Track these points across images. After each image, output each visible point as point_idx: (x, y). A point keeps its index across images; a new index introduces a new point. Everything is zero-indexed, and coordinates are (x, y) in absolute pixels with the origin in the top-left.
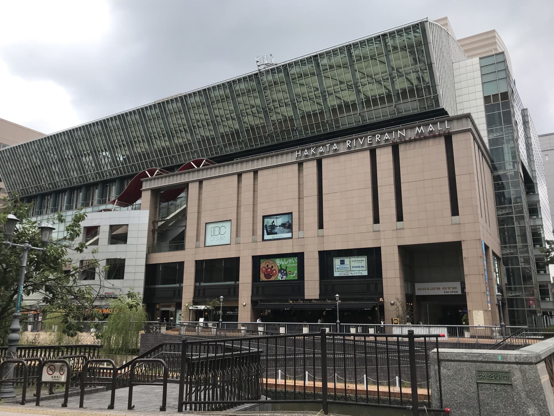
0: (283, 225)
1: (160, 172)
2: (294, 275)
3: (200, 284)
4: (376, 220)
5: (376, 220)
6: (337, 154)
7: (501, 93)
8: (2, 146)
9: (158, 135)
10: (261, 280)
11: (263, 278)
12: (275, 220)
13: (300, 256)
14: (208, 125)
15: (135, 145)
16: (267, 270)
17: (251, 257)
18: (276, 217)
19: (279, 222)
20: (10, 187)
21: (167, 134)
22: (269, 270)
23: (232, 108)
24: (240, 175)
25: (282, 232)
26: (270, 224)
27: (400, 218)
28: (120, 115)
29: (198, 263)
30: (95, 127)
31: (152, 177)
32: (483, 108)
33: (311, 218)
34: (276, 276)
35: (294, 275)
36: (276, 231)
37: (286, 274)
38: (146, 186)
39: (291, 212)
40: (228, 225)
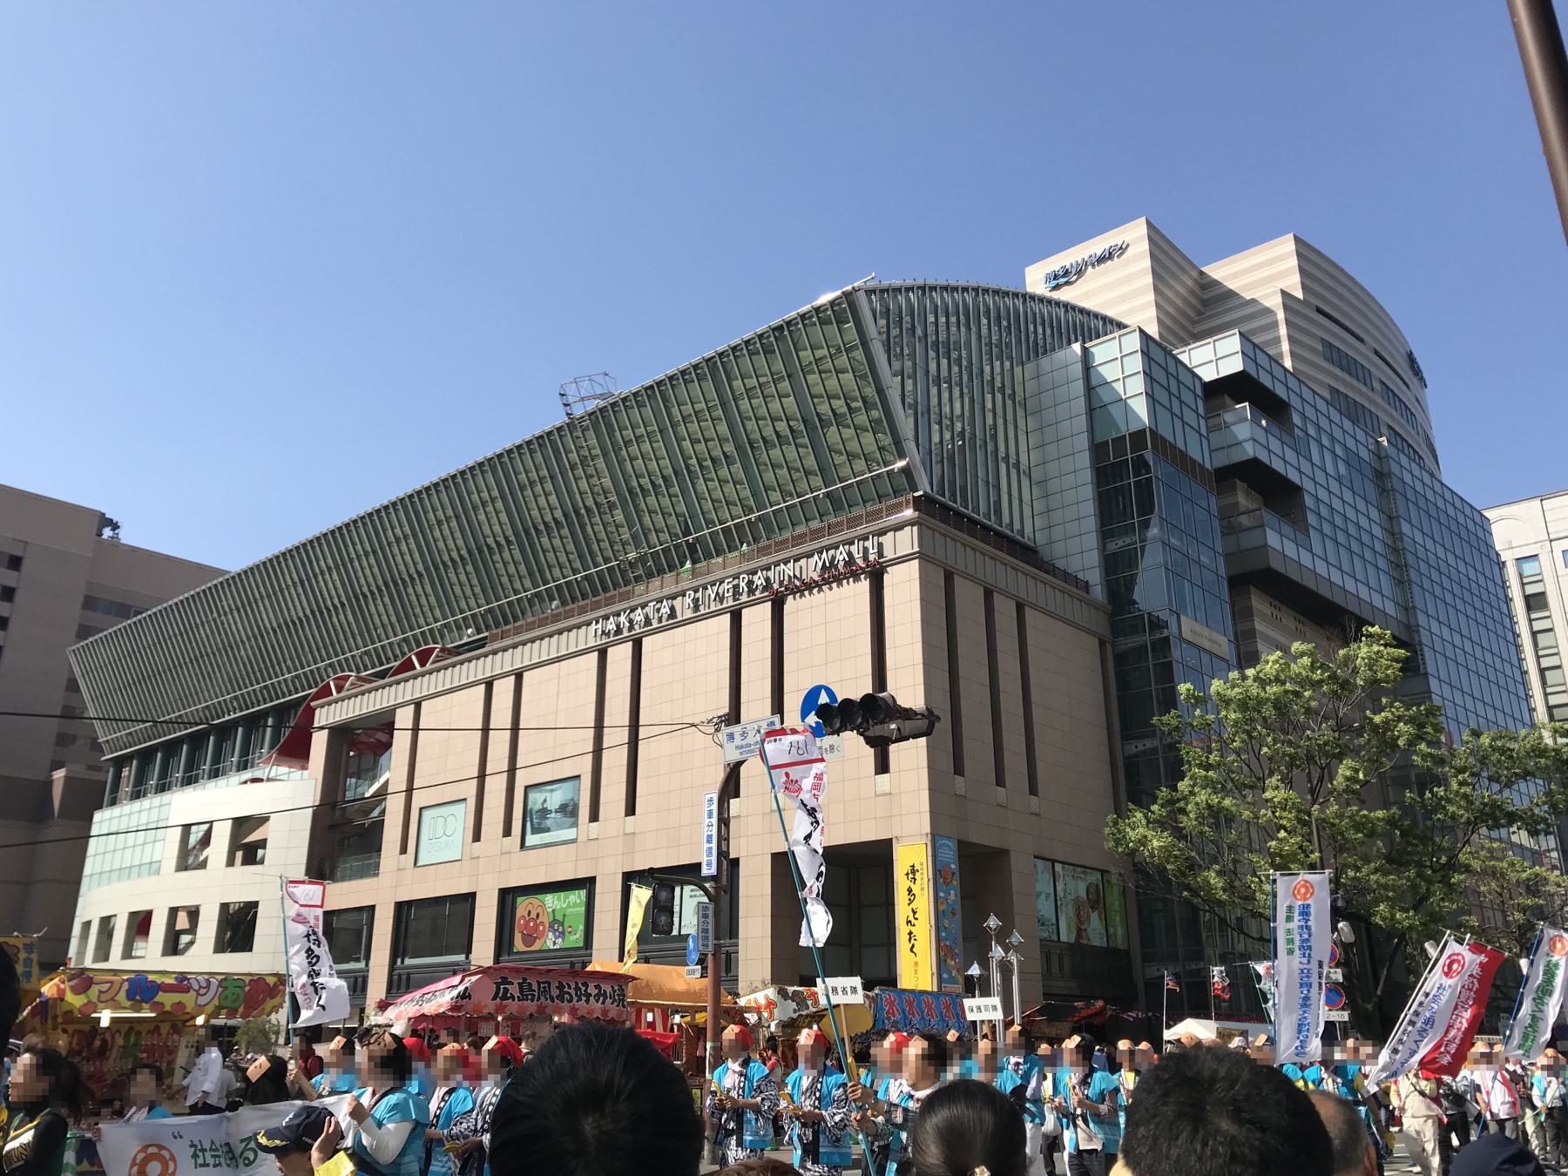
0: (563, 809)
2: (578, 936)
4: (477, 837)
5: (477, 837)
7: (1130, 435)
8: (132, 613)
9: (699, 463)
10: (515, 950)
11: (519, 945)
12: (548, 795)
13: (588, 884)
15: (538, 538)
16: (527, 923)
17: (769, 858)
18: (549, 787)
19: (555, 798)
21: (676, 477)
22: (532, 924)
25: (560, 827)
26: (538, 806)
27: (631, 810)
29: (402, 908)
31: (424, 669)
32: (1087, 475)
34: (542, 940)
35: (578, 936)
36: (549, 823)
37: (562, 934)
40: (461, 806)
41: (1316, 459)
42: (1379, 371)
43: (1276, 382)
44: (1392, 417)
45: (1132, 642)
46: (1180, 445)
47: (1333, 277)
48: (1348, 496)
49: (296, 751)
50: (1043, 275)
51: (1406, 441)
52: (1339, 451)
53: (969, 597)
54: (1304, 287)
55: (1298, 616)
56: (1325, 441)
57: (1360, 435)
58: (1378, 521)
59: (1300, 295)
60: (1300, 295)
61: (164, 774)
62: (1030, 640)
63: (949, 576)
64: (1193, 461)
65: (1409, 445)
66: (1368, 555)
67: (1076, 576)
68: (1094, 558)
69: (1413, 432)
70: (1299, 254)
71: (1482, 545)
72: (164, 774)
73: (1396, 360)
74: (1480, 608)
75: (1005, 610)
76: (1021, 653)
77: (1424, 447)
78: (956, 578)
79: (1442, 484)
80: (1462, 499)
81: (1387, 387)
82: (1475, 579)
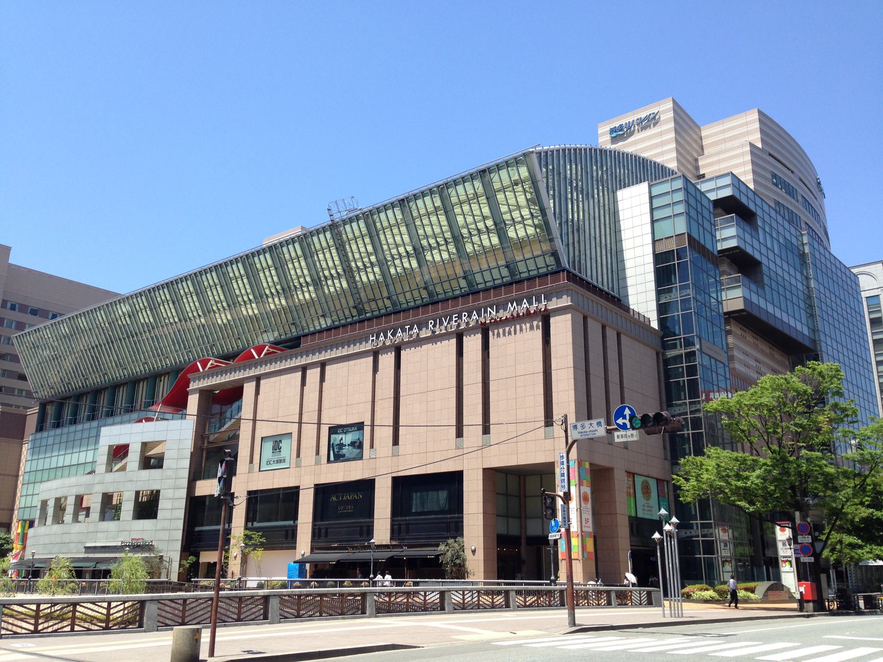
0: (353, 444)
1: (272, 350)
3: (252, 525)
6: (418, 342)
12: (344, 436)
14: (447, 243)
20: (73, 374)
23: (486, 211)
24: (304, 369)
26: (338, 442)
28: (272, 246)
30: (249, 260)
33: (384, 434)
38: (193, 386)
39: (363, 421)
41: (762, 240)
42: (801, 190)
43: (742, 194)
44: (807, 217)
45: (671, 353)
46: (702, 242)
47: (779, 135)
48: (785, 266)
49: (178, 403)
50: (608, 129)
51: (814, 231)
52: (781, 240)
53: (594, 328)
54: (763, 141)
55: (755, 335)
56: (774, 235)
57: (793, 230)
58: (801, 280)
59: (760, 145)
60: (760, 145)
61: (75, 413)
62: (623, 352)
63: (585, 318)
64: (708, 250)
65: (816, 233)
66: (795, 300)
67: (644, 316)
68: (653, 306)
69: (817, 225)
70: (760, 121)
71: (854, 292)
72: (75, 413)
73: (809, 181)
74: (852, 330)
75: (611, 335)
76: (619, 359)
77: (824, 234)
78: (622, 335)
79: (830, 253)
80: (840, 262)
81: (806, 199)
82: (840, 305)
